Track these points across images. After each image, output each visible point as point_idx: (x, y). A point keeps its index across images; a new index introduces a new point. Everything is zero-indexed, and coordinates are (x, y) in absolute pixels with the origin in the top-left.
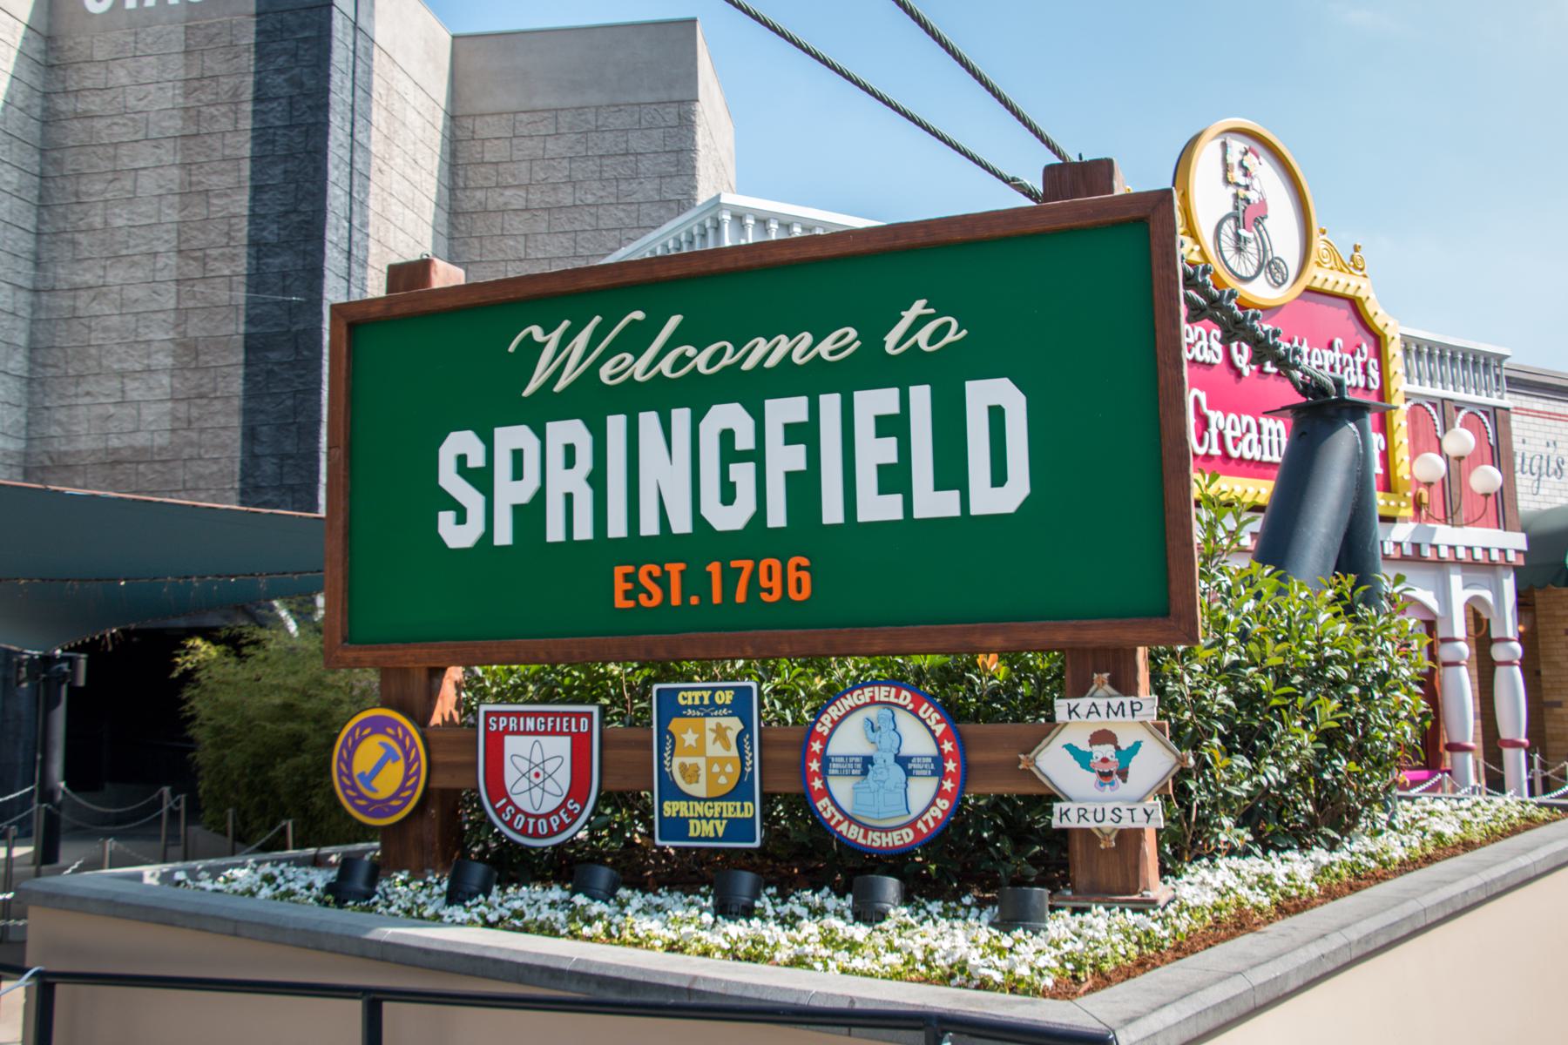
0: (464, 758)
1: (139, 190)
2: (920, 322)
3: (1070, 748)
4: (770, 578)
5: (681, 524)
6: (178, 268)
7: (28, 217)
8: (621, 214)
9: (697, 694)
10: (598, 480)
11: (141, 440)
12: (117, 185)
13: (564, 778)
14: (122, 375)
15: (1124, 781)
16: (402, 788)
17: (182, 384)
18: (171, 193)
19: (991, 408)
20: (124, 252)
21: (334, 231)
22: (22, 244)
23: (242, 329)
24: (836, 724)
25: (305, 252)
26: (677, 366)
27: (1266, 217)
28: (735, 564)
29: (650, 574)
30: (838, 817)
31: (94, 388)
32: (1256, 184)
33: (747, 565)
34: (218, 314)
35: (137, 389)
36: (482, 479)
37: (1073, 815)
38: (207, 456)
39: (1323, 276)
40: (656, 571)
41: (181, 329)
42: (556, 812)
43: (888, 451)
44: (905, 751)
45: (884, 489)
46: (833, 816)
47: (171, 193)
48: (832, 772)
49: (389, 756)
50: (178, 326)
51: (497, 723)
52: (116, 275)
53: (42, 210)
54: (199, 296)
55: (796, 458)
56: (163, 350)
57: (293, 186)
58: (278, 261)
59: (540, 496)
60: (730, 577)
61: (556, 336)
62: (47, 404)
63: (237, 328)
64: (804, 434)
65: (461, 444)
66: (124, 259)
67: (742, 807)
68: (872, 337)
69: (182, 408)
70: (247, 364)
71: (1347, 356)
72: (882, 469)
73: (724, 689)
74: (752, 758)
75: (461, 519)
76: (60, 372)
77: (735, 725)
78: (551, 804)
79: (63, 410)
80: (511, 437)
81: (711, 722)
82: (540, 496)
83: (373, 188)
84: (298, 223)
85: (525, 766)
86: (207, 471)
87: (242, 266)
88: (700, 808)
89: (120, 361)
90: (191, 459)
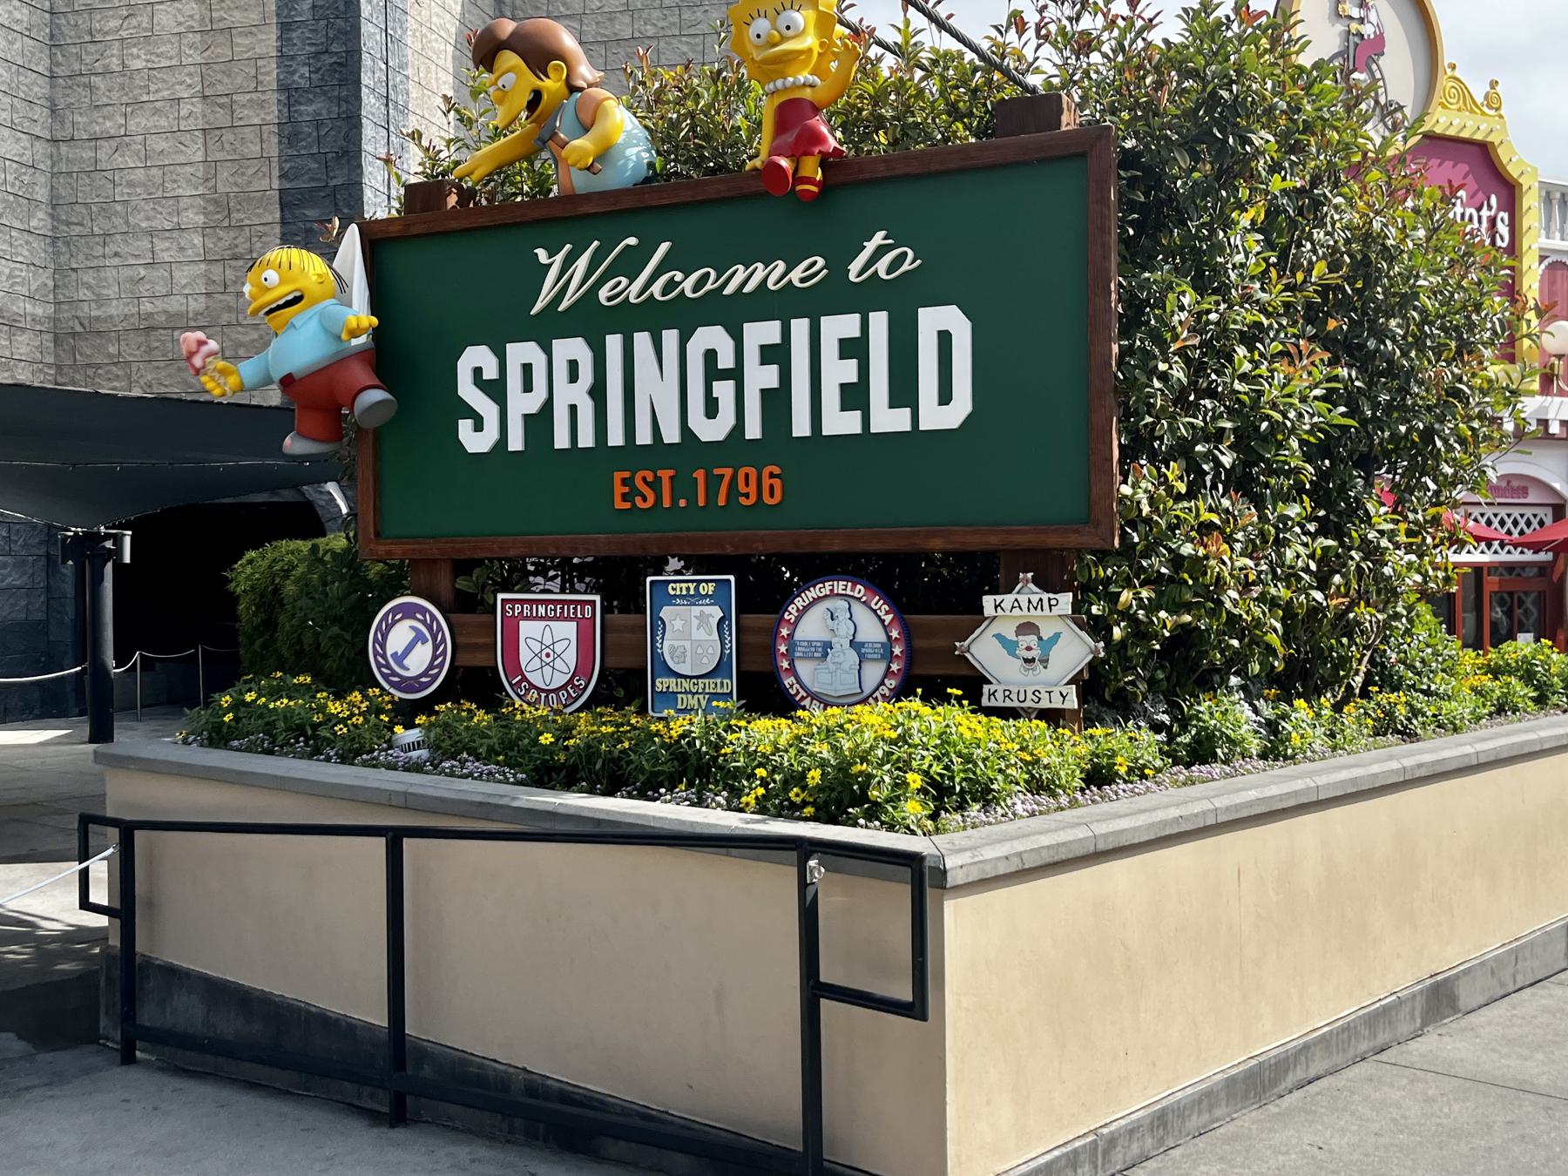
0: (488, 640)
1: (156, 28)
2: (880, 251)
3: (999, 637)
4: (747, 485)
5: (671, 435)
6: (204, 116)
7: (41, 59)
8: (685, 48)
9: (684, 585)
10: (598, 392)
11: (175, 304)
12: (134, 22)
13: (571, 657)
14: (151, 233)
15: (1045, 667)
16: (431, 667)
17: (215, 245)
18: (191, 30)
19: (940, 332)
20: (145, 98)
21: (369, 74)
22: (36, 89)
23: (276, 184)
24: (802, 612)
25: (339, 98)
26: (667, 289)
27: (1383, 54)
28: (717, 471)
29: (644, 479)
30: (803, 693)
31: (124, 249)
32: (1373, 16)
33: (727, 472)
34: (248, 167)
35: (168, 249)
36: (495, 390)
37: (999, 695)
38: (245, 322)
39: (1444, 121)
40: (650, 477)
41: (211, 184)
42: (564, 687)
43: (848, 371)
44: (859, 638)
45: (845, 406)
46: (798, 692)
47: (191, 30)
48: (797, 654)
49: (419, 638)
50: (207, 180)
51: (513, 609)
52: (138, 123)
53: (53, 49)
54: (227, 147)
55: (769, 376)
56: (192, 206)
57: (323, 23)
58: (310, 109)
59: (548, 404)
60: (713, 482)
61: (559, 258)
62: (74, 266)
63: (269, 183)
64: (776, 354)
65: (477, 357)
66: (146, 106)
67: (722, 683)
68: (838, 267)
69: (217, 270)
70: (283, 222)
71: (1471, 211)
72: (844, 387)
73: (707, 581)
74: (731, 642)
75: (479, 427)
76: (86, 231)
77: (717, 613)
78: (560, 680)
79: (91, 271)
80: (522, 352)
81: (696, 610)
82: (548, 404)
83: (411, 24)
84: (331, 65)
85: (537, 647)
86: (248, 338)
87: (272, 113)
88: (686, 684)
89: (148, 219)
90: (229, 325)
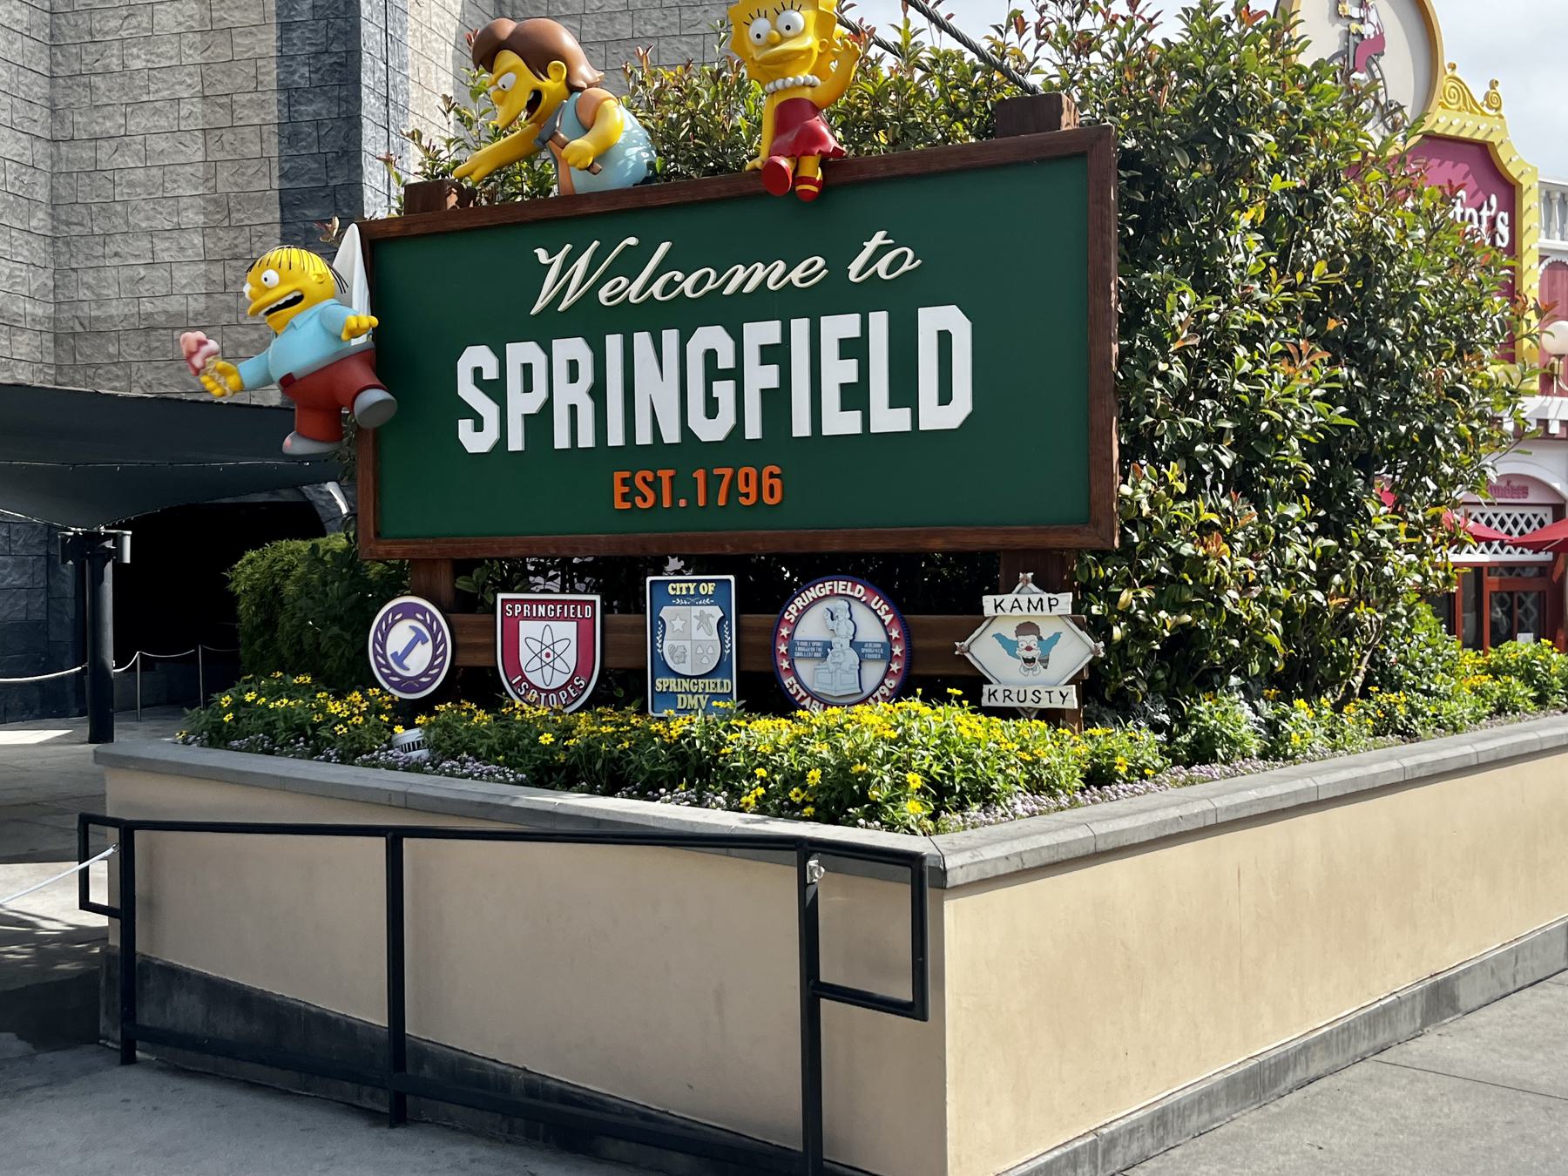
0: (488, 640)
1: (156, 28)
2: (880, 251)
3: (999, 637)
4: (747, 485)
5: (671, 435)
6: (204, 116)
7: (41, 59)
8: (685, 48)
9: (684, 585)
10: (598, 392)
11: (175, 304)
12: (134, 22)
13: (571, 657)
14: (151, 233)
15: (1045, 667)
16: (431, 667)
17: (215, 245)
18: (191, 30)
19: (940, 332)
20: (145, 98)
21: (369, 74)
22: (36, 89)
23: (276, 184)
24: (802, 612)
25: (339, 98)
26: (667, 289)
27: (1383, 54)
28: (717, 471)
29: (644, 479)
30: (803, 693)
31: (124, 249)
32: (1373, 16)
33: (727, 472)
34: (248, 167)
35: (168, 249)
36: (495, 390)
37: (999, 695)
38: (245, 322)
39: (1444, 121)
40: (650, 477)
41: (211, 184)
42: (564, 687)
43: (848, 371)
44: (859, 638)
45: (845, 406)
46: (798, 692)
47: (191, 30)
48: (797, 654)
49: (419, 638)
50: (207, 180)
51: (513, 609)
52: (138, 123)
53: (53, 49)
54: (227, 147)
55: (769, 376)
56: (192, 206)
57: (323, 23)
58: (310, 109)
59: (548, 404)
60: (713, 482)
61: (559, 258)
62: (74, 266)
63: (269, 183)
64: (776, 354)
65: (477, 357)
66: (146, 106)
67: (722, 683)
68: (838, 267)
69: (217, 270)
70: (283, 222)
71: (1471, 211)
72: (844, 387)
73: (707, 581)
74: (731, 642)
75: (479, 427)
76: (86, 231)
77: (717, 613)
78: (560, 680)
79: (91, 271)
80: (522, 352)
81: (696, 610)
82: (548, 404)
83: (411, 24)
84: (331, 65)
85: (537, 647)
86: (248, 338)
87: (272, 113)
88: (686, 684)
89: (148, 219)
90: (229, 325)
